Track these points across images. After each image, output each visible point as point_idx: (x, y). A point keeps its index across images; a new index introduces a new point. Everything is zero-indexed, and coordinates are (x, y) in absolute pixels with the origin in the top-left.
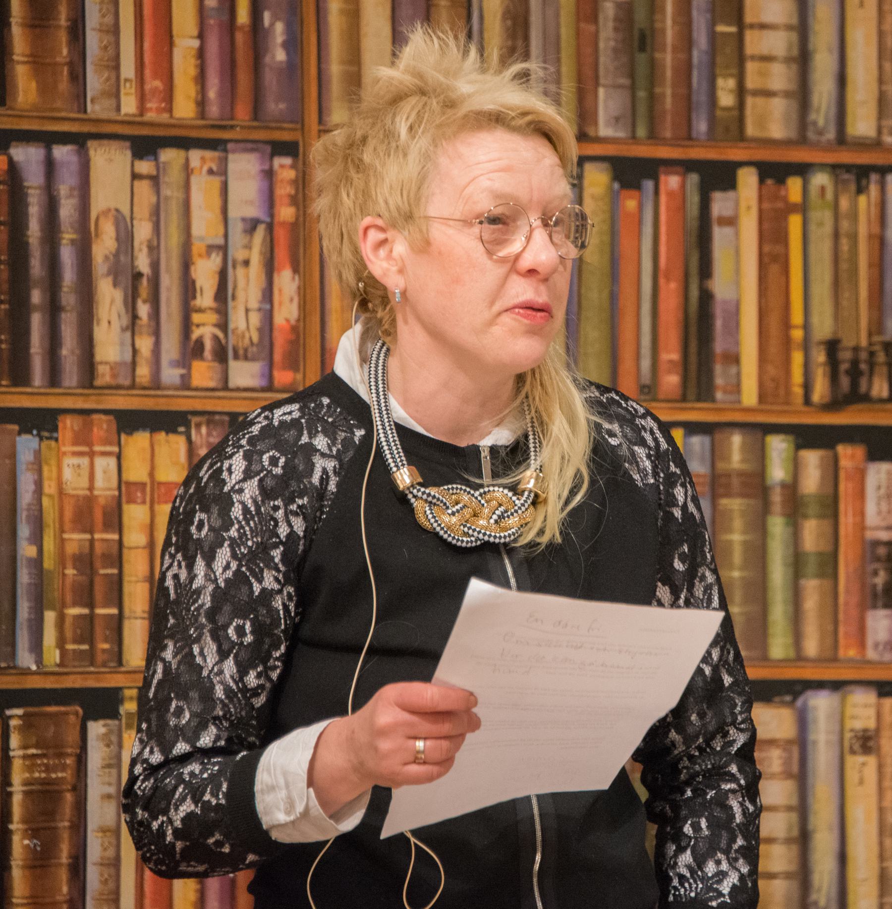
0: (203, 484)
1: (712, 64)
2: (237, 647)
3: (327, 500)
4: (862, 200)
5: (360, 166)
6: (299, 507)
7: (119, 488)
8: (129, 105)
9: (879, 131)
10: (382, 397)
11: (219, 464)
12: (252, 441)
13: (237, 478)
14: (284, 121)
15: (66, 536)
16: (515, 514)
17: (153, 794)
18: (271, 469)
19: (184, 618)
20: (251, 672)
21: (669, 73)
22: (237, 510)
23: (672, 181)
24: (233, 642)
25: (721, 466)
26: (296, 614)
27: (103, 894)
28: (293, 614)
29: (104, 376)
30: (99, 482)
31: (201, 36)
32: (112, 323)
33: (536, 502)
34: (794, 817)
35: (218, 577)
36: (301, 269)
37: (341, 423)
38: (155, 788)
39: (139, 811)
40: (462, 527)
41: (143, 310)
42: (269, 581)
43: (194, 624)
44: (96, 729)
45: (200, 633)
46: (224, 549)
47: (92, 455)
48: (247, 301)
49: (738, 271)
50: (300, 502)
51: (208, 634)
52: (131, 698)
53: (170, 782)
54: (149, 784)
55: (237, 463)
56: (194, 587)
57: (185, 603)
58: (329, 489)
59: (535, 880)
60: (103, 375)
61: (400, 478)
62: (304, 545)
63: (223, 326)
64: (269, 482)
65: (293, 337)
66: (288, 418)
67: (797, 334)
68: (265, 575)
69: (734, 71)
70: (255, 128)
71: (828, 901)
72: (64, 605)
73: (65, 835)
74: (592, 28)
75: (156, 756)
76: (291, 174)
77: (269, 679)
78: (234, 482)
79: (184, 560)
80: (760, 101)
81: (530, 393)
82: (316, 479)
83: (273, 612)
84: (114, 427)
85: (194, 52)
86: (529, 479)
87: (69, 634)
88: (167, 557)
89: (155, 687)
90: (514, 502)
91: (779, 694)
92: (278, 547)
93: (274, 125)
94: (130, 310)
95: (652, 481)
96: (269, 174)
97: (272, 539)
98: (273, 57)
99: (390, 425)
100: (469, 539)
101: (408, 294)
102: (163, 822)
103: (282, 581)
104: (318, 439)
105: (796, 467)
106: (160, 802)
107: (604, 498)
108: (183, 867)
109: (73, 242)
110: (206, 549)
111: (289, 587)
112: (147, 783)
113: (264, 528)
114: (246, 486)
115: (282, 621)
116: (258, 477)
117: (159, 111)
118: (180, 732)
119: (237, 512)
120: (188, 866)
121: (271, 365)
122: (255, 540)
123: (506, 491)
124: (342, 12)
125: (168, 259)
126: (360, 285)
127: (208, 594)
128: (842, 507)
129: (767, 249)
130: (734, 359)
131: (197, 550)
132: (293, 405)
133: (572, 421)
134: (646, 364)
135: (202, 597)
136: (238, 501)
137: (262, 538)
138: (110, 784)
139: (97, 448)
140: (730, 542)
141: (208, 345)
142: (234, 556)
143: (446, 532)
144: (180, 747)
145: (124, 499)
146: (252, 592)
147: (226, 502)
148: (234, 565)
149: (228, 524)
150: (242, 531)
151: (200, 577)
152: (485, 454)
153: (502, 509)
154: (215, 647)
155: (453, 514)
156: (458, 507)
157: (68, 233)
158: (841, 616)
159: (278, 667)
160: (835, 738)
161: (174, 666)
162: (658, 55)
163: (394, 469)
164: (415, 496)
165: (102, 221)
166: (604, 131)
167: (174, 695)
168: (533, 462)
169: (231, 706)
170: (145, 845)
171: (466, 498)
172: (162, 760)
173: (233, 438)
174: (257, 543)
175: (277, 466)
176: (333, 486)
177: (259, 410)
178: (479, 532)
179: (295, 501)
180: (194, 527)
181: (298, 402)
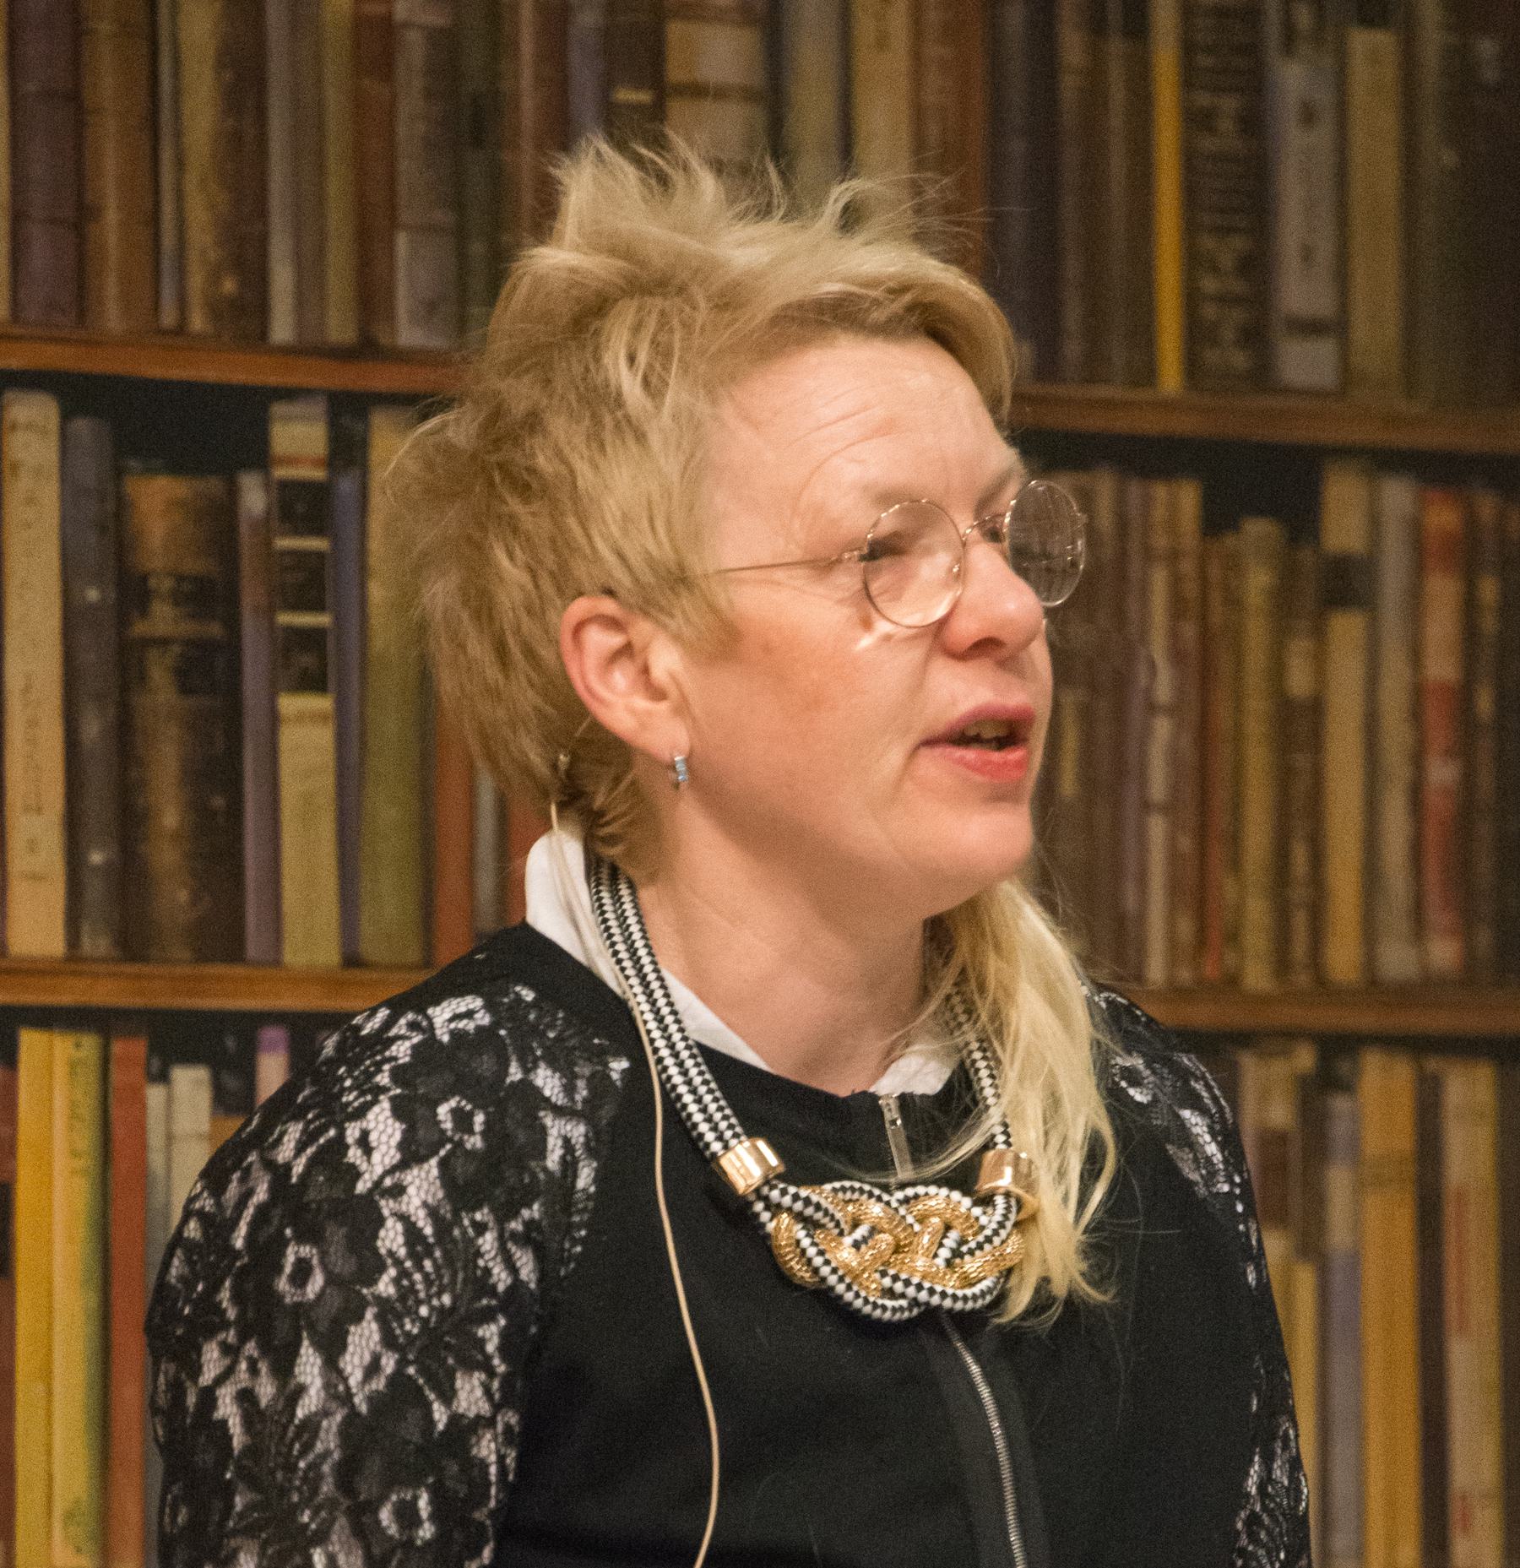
0: (294, 1180)
3: (580, 1212)
5: (527, 486)
11: (332, 1133)
12: (399, 1075)
13: (387, 1161)
18: (461, 1139)
22: (391, 1234)
35: (354, 1390)
42: (471, 1395)
46: (364, 1324)
55: (381, 1127)
64: (460, 1168)
66: (468, 1025)
68: (459, 1383)
78: (379, 1170)
82: (553, 1160)
92: (493, 1319)
97: (480, 1299)
103: (497, 1396)
110: (322, 1327)
111: (510, 1414)
119: (391, 1238)
132: (469, 999)
142: (389, 1340)
146: (431, 1423)
148: (389, 1363)
149: (372, 1266)
150: (405, 1282)
151: (313, 1391)
152: (892, 1114)
153: (954, 1235)
171: (876, 1209)
174: (441, 1310)
175: (471, 1132)
178: (919, 1287)
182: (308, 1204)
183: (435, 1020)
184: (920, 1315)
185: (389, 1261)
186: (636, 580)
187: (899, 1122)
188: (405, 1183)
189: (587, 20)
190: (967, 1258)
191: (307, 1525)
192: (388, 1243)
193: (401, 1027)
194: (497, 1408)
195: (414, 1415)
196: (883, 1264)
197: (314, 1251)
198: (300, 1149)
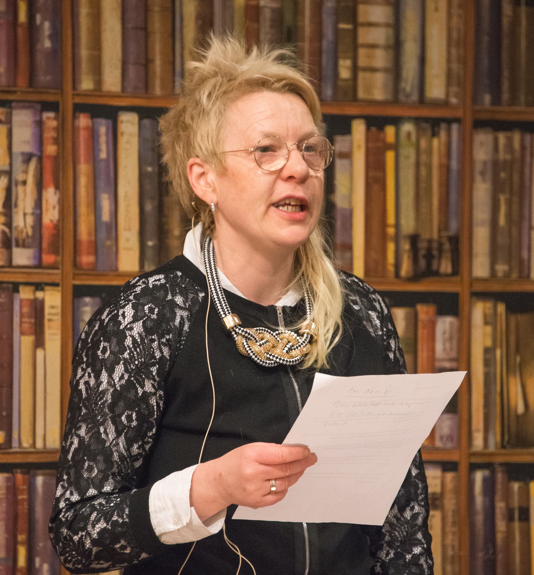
3: (184, 337)
4: (435, 142)
9: (448, 94)
11: (116, 312)
13: (129, 320)
16: (299, 348)
18: (150, 315)
19: (93, 410)
22: (129, 341)
24: (125, 425)
35: (116, 384)
36: (61, 187)
38: (75, 517)
40: (266, 354)
45: (104, 419)
46: (120, 365)
48: (24, 208)
49: (351, 189)
50: (168, 337)
51: (110, 420)
53: (85, 510)
54: (70, 514)
55: (128, 311)
56: (100, 389)
61: (227, 321)
64: (150, 324)
65: (55, 232)
66: (158, 283)
68: (146, 383)
69: (350, 54)
74: (255, 26)
75: (75, 497)
76: (54, 124)
77: (144, 449)
78: (126, 323)
79: (93, 372)
80: (367, 75)
81: (305, 271)
83: (149, 406)
89: (73, 453)
90: (298, 340)
92: (155, 366)
93: (43, 90)
96: (40, 124)
98: (43, 45)
100: (270, 362)
101: (219, 205)
102: (82, 536)
104: (177, 297)
111: (161, 391)
112: (69, 513)
114: (135, 326)
115: (156, 413)
116: (142, 320)
118: (91, 483)
119: (128, 342)
122: (140, 360)
123: (293, 333)
124: (89, 15)
127: (110, 394)
129: (371, 174)
132: (160, 275)
133: (331, 288)
136: (129, 335)
142: (126, 370)
143: (256, 357)
144: (91, 492)
147: (121, 336)
148: (126, 377)
150: (132, 354)
151: (104, 383)
153: (290, 344)
154: (114, 428)
156: (263, 341)
159: (150, 442)
161: (87, 440)
163: (223, 316)
164: (236, 333)
168: (308, 316)
170: (67, 552)
172: (79, 499)
173: (123, 295)
174: (142, 362)
175: (154, 314)
176: (187, 328)
178: (277, 358)
179: (165, 336)
180: (100, 352)
182: (108, 331)
183: (149, 281)
184: (277, 366)
185: (128, 348)
188: (133, 327)
189: (329, 4)
190: (293, 350)
193: (140, 283)
194: (157, 390)
195: (133, 391)
196: (268, 351)
197: (108, 344)
198: (107, 316)
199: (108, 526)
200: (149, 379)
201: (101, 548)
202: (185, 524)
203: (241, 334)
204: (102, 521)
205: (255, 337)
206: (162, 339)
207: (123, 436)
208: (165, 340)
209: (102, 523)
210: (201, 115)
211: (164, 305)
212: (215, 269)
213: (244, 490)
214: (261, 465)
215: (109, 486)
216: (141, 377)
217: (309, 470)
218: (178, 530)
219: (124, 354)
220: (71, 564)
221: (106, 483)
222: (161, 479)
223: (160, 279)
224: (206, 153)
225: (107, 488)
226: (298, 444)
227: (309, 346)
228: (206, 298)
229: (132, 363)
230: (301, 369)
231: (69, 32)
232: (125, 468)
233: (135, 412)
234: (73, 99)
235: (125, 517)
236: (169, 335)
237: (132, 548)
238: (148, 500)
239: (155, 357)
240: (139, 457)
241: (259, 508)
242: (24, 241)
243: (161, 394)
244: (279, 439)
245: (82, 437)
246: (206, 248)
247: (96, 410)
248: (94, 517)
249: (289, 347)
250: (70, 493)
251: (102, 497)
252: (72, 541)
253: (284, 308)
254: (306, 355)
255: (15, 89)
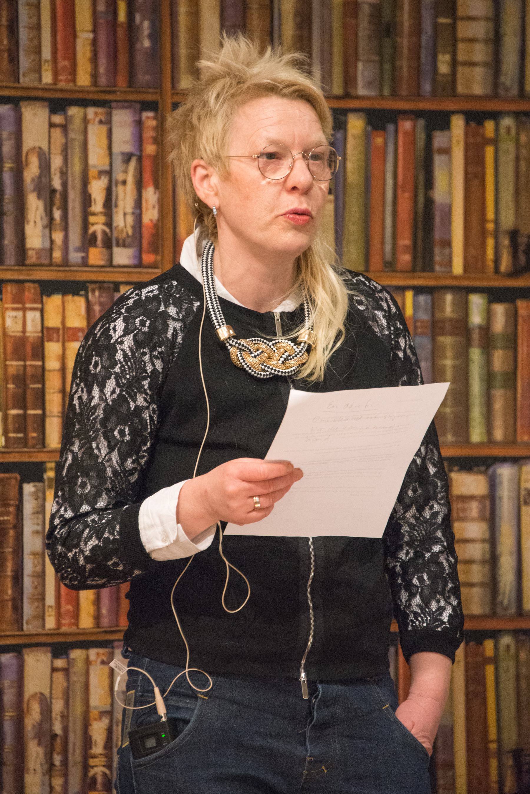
1: (435, 45)
2: (120, 443)
3: (176, 349)
6: (159, 353)
7: (42, 331)
8: (47, 78)
10: (210, 279)
11: (107, 325)
12: (128, 310)
13: (120, 334)
14: (149, 88)
15: (8, 363)
16: (295, 358)
17: (68, 536)
18: (141, 328)
19: (86, 425)
20: (129, 459)
21: (405, 52)
22: (119, 355)
23: (407, 125)
24: (117, 440)
25: (438, 315)
26: (158, 422)
27: (35, 595)
28: (156, 422)
29: (32, 257)
30: (30, 327)
31: (94, 31)
32: (37, 222)
33: (309, 350)
34: (487, 546)
35: (108, 398)
36: (160, 186)
37: (184, 298)
38: (69, 532)
39: (59, 547)
40: (261, 365)
41: (57, 214)
42: (141, 401)
43: (92, 428)
44: (29, 488)
46: (111, 380)
47: (24, 310)
48: (124, 208)
49: (450, 185)
50: (160, 350)
51: (102, 435)
52: (51, 469)
53: (79, 527)
55: (119, 324)
56: (92, 404)
57: (86, 415)
58: (178, 341)
59: (309, 590)
60: (31, 257)
62: (163, 378)
63: (109, 224)
65: (154, 232)
66: (151, 294)
67: (490, 226)
68: (138, 397)
70: (132, 92)
71: (510, 602)
72: (7, 408)
73: (10, 557)
74: (354, 22)
75: (69, 513)
76: (153, 123)
77: (139, 464)
78: (117, 337)
79: (85, 387)
80: (467, 69)
84: (39, 291)
85: (89, 42)
86: (304, 334)
87: (10, 426)
88: (74, 386)
89: (67, 469)
90: (295, 349)
91: (478, 466)
92: (147, 379)
93: (141, 90)
94: (48, 213)
95: (387, 333)
96: (139, 124)
97: (142, 374)
98: (142, 44)
99: (215, 298)
102: (76, 553)
103: (149, 400)
104: (170, 308)
105: (489, 315)
106: (72, 540)
107: (355, 346)
108: (89, 582)
109: (11, 169)
110: (100, 380)
111: (154, 405)
112: (63, 530)
113: (138, 367)
115: (149, 427)
116: (133, 334)
117: (67, 81)
118: (85, 499)
119: (119, 356)
120: (93, 580)
121: (140, 251)
122: (131, 374)
123: (290, 342)
124: (188, 13)
125: (73, 181)
126: (196, 205)
127: (101, 409)
128: (520, 342)
129: (470, 169)
130: (448, 243)
131: (94, 380)
132: (154, 286)
134: (388, 248)
135: (97, 411)
137: (136, 373)
138: (38, 524)
139: (28, 305)
140: (444, 366)
141: (99, 237)
142: (118, 384)
144: (84, 508)
145: (45, 338)
147: (112, 350)
148: (118, 391)
149: (114, 363)
150: (123, 368)
151: (96, 398)
152: (277, 317)
153: (287, 354)
154: (106, 443)
155: (255, 357)
156: (258, 352)
157: (8, 163)
158: (519, 414)
159: (145, 456)
160: (515, 494)
161: (80, 455)
162: (398, 39)
163: (218, 327)
164: (231, 345)
165: (30, 155)
166: (362, 91)
167: (81, 474)
168: (306, 323)
169: (117, 482)
170: (63, 569)
172: (73, 516)
173: (116, 308)
174: (133, 376)
175: (145, 327)
176: (180, 339)
177: (132, 290)
178: (272, 369)
179: (157, 349)
180: (92, 366)
181: (157, 284)
182: (99, 345)
184: (273, 377)
185: (119, 362)
186: (208, 157)
187: (279, 320)
190: (290, 360)
191: (91, 435)
192: (118, 358)
195: (125, 406)
197: (99, 359)
199: (100, 544)
200: (141, 392)
201: (94, 565)
202: (172, 542)
203: (235, 346)
204: (94, 538)
205: (250, 348)
206: (153, 352)
207: (116, 451)
208: (157, 352)
209: (94, 540)
210: (208, 116)
211: (156, 317)
212: (212, 278)
213: (228, 507)
214: (244, 483)
215: (102, 501)
216: (133, 391)
217: (296, 484)
218: (167, 547)
219: (115, 368)
220: (68, 581)
221: (99, 499)
222: (151, 495)
223: (154, 290)
224: (211, 156)
225: (101, 504)
226: (280, 460)
227: (306, 355)
228: (201, 308)
229: (124, 377)
230: (295, 380)
231: (168, 31)
232: (119, 483)
233: (128, 427)
234: (172, 98)
235: (116, 534)
236: (162, 348)
237: (124, 565)
238: (138, 516)
239: (146, 370)
240: (134, 472)
241: (245, 525)
242: (124, 241)
243: (155, 407)
244: (262, 455)
245: (76, 453)
246: (205, 256)
247: (88, 425)
248: (86, 534)
249: (285, 357)
250: (64, 510)
251: (95, 513)
252: (67, 558)
253: (282, 314)
254: (303, 364)
255: (114, 89)
